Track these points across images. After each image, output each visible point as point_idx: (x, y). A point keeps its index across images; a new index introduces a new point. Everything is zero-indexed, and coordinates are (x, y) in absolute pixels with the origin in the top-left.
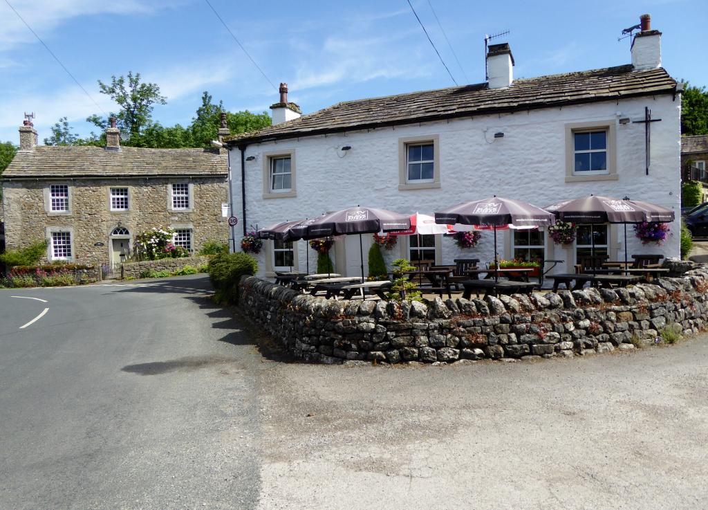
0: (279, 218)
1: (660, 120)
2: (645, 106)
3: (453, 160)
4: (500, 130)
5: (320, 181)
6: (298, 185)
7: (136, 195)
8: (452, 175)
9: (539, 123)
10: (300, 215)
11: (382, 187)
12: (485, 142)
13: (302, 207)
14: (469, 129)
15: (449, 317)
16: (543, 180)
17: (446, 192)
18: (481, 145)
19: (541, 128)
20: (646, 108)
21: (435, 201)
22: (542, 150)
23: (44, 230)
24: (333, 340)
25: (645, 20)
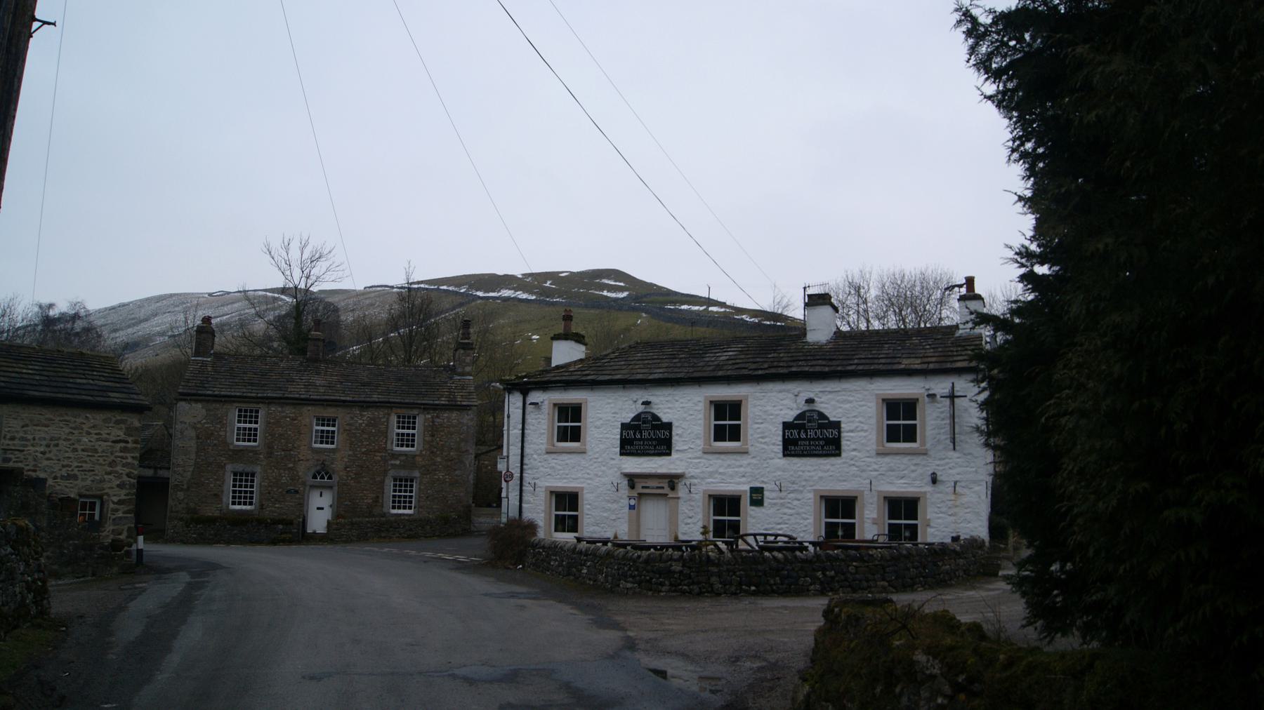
0: (564, 476)
1: (965, 396)
2: (952, 381)
3: (762, 423)
4: (812, 395)
5: (613, 437)
6: (588, 439)
7: (347, 428)
8: (760, 440)
10: (588, 474)
11: (686, 447)
13: (592, 465)
14: (780, 392)
15: (734, 565)
16: (854, 450)
17: (754, 457)
19: (853, 396)
20: (953, 384)
21: (741, 466)
22: (853, 419)
23: (222, 467)
24: (651, 579)
25: (970, 282)
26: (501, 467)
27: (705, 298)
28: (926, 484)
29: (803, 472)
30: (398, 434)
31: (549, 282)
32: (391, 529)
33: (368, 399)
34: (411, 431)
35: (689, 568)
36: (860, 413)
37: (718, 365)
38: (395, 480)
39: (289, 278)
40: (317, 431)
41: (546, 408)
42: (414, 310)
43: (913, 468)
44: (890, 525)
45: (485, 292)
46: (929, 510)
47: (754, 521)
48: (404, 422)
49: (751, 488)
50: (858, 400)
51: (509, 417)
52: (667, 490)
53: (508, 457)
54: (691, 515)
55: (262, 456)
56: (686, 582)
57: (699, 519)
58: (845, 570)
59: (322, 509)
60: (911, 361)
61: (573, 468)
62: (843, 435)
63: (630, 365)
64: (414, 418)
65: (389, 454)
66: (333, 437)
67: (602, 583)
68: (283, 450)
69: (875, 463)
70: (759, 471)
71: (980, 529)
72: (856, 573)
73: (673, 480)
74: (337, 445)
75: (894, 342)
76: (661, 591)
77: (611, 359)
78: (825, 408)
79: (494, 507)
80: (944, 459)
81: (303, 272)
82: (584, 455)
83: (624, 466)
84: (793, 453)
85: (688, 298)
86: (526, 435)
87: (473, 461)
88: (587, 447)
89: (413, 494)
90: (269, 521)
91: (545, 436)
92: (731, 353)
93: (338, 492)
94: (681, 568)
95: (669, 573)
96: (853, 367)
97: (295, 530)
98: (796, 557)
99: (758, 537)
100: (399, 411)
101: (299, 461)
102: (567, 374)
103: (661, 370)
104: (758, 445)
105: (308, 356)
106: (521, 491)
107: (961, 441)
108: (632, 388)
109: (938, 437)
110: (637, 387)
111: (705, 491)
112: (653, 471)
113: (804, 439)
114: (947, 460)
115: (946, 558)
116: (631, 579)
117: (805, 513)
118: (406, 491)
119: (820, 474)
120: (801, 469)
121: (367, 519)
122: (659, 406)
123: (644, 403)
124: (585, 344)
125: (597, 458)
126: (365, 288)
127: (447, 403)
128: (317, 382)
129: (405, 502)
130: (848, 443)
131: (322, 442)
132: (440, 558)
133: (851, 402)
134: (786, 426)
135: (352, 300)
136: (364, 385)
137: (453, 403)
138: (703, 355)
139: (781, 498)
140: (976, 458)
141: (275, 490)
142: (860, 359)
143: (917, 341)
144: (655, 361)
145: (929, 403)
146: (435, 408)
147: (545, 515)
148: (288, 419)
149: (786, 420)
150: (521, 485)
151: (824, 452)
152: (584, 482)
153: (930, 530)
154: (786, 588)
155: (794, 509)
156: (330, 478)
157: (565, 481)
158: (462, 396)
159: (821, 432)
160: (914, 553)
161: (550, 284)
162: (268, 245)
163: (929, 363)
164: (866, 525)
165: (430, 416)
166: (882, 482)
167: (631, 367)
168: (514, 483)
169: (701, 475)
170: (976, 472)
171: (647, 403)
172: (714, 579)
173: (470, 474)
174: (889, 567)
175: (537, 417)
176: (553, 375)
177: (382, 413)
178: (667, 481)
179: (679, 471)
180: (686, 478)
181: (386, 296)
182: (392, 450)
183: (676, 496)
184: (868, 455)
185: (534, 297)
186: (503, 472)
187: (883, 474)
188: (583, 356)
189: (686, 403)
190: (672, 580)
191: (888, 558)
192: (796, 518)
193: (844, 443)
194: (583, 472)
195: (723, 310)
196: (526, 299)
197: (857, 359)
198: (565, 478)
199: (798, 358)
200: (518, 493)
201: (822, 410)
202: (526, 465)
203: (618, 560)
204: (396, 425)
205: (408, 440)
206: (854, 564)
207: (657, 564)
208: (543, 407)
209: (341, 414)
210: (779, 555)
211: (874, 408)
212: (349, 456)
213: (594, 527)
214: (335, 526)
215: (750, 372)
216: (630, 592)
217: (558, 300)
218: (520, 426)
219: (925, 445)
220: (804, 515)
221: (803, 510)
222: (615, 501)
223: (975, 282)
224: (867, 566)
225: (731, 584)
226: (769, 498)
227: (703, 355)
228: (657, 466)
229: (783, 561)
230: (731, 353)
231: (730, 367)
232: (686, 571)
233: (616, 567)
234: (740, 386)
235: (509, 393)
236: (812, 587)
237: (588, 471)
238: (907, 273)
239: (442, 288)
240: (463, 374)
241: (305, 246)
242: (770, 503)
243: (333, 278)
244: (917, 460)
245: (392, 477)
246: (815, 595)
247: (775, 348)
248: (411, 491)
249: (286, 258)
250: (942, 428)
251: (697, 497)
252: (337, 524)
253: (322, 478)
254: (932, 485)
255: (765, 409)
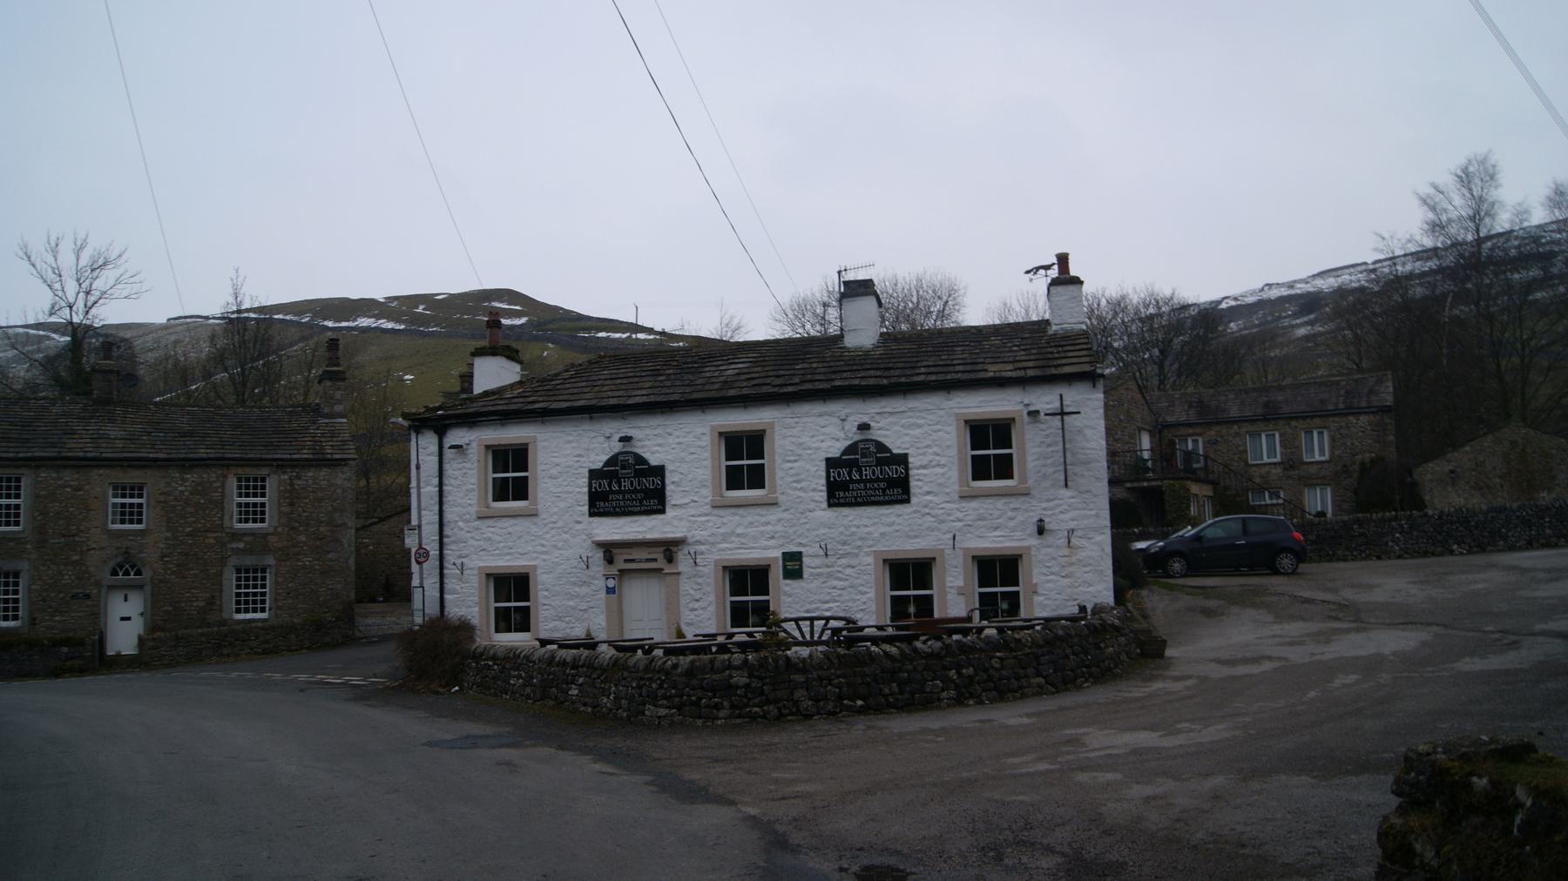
0: (506, 551)
1: (1079, 413)
2: (1059, 393)
3: (796, 461)
4: (865, 419)
5: (578, 490)
6: (540, 495)
7: (162, 498)
8: (795, 485)
9: (921, 411)
10: (543, 546)
11: (686, 501)
12: (844, 436)
13: (547, 533)
16: (929, 493)
17: (787, 510)
18: (838, 440)
19: (923, 418)
20: (1061, 396)
22: (926, 450)
25: (1063, 260)
26: (411, 541)
27: (632, 323)
28: (1030, 535)
29: (858, 527)
30: (240, 505)
31: (421, 307)
32: (237, 643)
33: (191, 456)
34: (259, 500)
35: (760, 678)
36: (934, 441)
37: (726, 382)
38: (238, 571)
39: (60, 293)
40: (115, 505)
41: (475, 452)
42: (246, 338)
43: (1010, 514)
44: (981, 594)
45: (336, 322)
46: (1035, 571)
47: (790, 599)
48: (247, 487)
49: (783, 553)
50: (930, 423)
51: (418, 467)
52: (661, 563)
53: (420, 526)
54: (697, 597)
55: (28, 546)
56: (756, 701)
57: (711, 603)
58: (987, 665)
59: (128, 619)
60: (1001, 367)
61: (519, 538)
62: (912, 472)
63: (596, 386)
64: (263, 480)
65: (227, 533)
66: (140, 514)
67: (610, 710)
68: (63, 536)
69: (958, 509)
70: (794, 529)
71: (1105, 592)
72: (1003, 668)
73: (670, 548)
74: (147, 525)
75: (967, 343)
76: (717, 718)
77: (565, 379)
78: (885, 436)
79: (381, 602)
80: (1052, 500)
81: (80, 285)
82: (535, 519)
83: (596, 531)
84: (602, 510)
85: (605, 324)
86: (445, 493)
87: (353, 538)
88: (539, 507)
89: (267, 590)
90: (45, 642)
91: (475, 493)
92: (741, 366)
93: (152, 595)
94: (748, 680)
95: (729, 688)
96: (922, 378)
97: (89, 654)
98: (915, 650)
99: (800, 623)
100: (240, 471)
101: (89, 550)
102: (503, 402)
103: (644, 392)
104: (790, 492)
105: (95, 396)
106: (442, 576)
107: (1075, 474)
108: (604, 417)
109: (1043, 470)
110: (610, 417)
111: (716, 561)
112: (640, 537)
113: (858, 482)
114: (1057, 502)
115: (1108, 637)
116: (665, 702)
117: (863, 585)
118: (255, 587)
119: (883, 529)
120: (854, 523)
121: (200, 631)
122: (644, 443)
123: (622, 440)
124: (519, 362)
125: (555, 523)
126: (169, 320)
127: (311, 456)
128: (111, 433)
129: (255, 602)
130: (920, 483)
131: (123, 522)
132: (322, 683)
133: (920, 426)
134: (831, 463)
135: (151, 335)
136: (184, 435)
137: (321, 456)
138: (700, 370)
139: (828, 566)
140: (1095, 496)
141: (53, 595)
142: (929, 366)
143: (997, 342)
144: (632, 380)
145: (1030, 423)
146: (294, 464)
147: (480, 608)
148: (68, 490)
149: (830, 455)
150: (442, 567)
151: (887, 498)
152: (537, 558)
153: (1037, 599)
154: (908, 699)
155: (847, 580)
156: (138, 573)
157: (509, 557)
158: (332, 446)
159: (881, 469)
160: (1073, 633)
161: (423, 309)
162: (26, 246)
163: (1025, 369)
164: (949, 597)
165: (286, 477)
166: (969, 535)
167: (596, 388)
168: (431, 565)
169: (711, 539)
170: (1097, 516)
171: (626, 439)
172: (800, 694)
173: (349, 558)
174: (1043, 655)
175: (460, 466)
176: (481, 404)
177: (214, 475)
178: (662, 549)
179: (678, 535)
180: (689, 544)
181: (199, 330)
182: (232, 528)
183: (676, 571)
184: (948, 500)
185: (402, 327)
186: (414, 550)
187: (969, 525)
188: (517, 378)
189: (684, 437)
190: (733, 698)
191: (1041, 642)
192: (850, 593)
193: (913, 483)
194: (534, 544)
195: (652, 337)
196: (392, 329)
197: (924, 367)
198: (508, 554)
199: (839, 369)
200: (437, 579)
201: (880, 439)
202: (448, 537)
203: (637, 672)
204: (235, 491)
205: (255, 513)
206: (998, 654)
207: (708, 676)
208: (470, 451)
209: (153, 481)
210: (893, 650)
211: (954, 434)
212: (167, 539)
213: (556, 623)
214: (151, 644)
215: (776, 390)
216: (665, 723)
217: (434, 329)
218: (436, 481)
219: (1026, 482)
220: (861, 588)
221: (859, 581)
222: (585, 582)
223: (1070, 261)
224: (1015, 657)
225: (826, 699)
226: (809, 567)
227: (700, 370)
228: (644, 529)
229: (898, 657)
230: (741, 366)
231: (745, 384)
232: (756, 684)
233: (634, 685)
234: (762, 409)
235: (417, 433)
236: (945, 694)
237: (543, 542)
238: (901, 280)
239: (276, 317)
240: (332, 416)
241: (82, 248)
242: (812, 574)
243: (125, 293)
244: (1015, 503)
245: (234, 566)
246: (949, 706)
247: (802, 357)
248: (264, 586)
249: (54, 265)
250: (1048, 458)
251: (706, 570)
252: (154, 639)
253: (127, 573)
254: (1038, 536)
255: (801, 440)
